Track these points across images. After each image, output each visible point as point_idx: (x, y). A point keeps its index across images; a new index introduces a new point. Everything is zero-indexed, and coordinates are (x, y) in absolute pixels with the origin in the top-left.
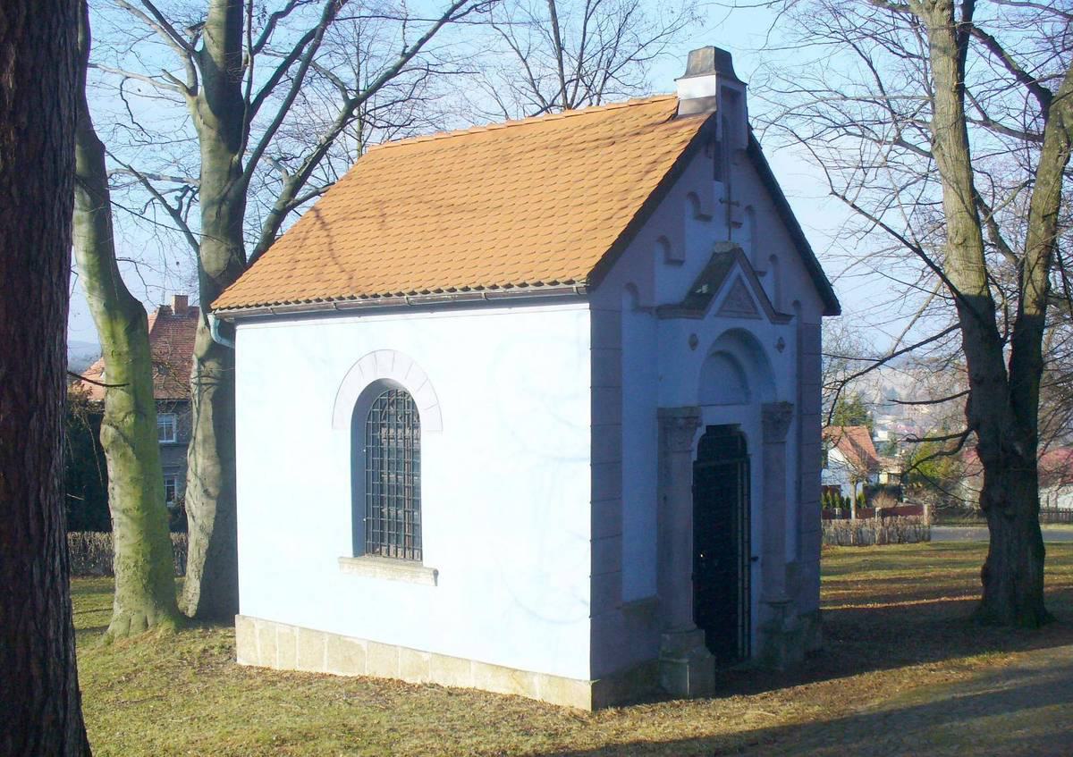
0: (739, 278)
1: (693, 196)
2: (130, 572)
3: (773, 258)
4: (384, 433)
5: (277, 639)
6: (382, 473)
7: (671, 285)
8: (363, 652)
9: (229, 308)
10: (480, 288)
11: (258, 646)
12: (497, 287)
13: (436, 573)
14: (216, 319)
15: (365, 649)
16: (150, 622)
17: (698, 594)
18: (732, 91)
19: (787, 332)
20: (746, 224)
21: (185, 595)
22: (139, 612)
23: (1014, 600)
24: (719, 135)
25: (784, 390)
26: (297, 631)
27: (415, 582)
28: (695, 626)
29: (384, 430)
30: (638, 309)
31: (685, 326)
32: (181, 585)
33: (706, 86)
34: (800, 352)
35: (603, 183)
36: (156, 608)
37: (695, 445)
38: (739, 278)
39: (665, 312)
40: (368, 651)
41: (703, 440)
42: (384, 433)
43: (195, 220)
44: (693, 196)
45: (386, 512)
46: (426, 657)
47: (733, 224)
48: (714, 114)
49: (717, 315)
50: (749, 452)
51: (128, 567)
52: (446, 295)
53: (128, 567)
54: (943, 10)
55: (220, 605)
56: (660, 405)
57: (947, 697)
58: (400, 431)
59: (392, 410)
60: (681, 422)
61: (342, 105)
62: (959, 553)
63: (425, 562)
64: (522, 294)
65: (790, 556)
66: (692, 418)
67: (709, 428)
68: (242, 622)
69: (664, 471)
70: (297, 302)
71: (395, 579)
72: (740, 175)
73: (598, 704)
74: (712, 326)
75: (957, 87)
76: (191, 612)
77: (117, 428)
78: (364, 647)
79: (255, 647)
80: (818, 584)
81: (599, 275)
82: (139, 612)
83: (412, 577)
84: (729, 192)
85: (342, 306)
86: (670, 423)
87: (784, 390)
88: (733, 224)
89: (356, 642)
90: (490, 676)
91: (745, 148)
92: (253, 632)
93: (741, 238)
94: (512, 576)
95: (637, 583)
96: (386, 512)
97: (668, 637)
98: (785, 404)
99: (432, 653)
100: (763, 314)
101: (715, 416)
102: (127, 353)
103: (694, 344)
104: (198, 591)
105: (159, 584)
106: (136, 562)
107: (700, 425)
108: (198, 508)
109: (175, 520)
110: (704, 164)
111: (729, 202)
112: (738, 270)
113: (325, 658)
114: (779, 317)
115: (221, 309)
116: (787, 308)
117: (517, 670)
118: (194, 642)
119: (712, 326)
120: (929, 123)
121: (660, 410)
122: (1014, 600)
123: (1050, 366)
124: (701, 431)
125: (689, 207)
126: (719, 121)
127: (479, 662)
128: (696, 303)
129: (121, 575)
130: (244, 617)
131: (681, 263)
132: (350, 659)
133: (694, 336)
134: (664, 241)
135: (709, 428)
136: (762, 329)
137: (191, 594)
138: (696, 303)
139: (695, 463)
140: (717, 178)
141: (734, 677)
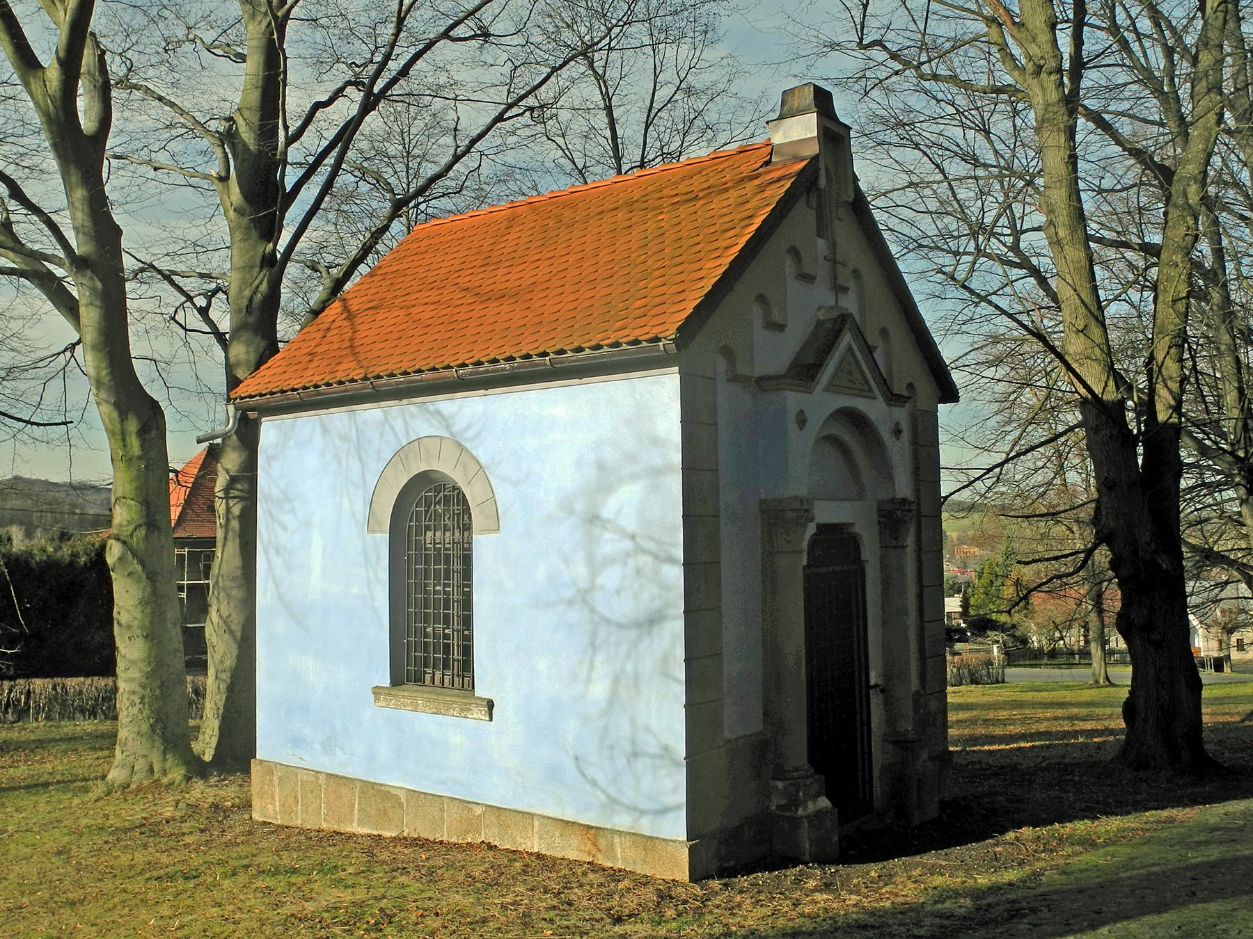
0: (850, 349)
1: (794, 252)
2: (135, 710)
3: (884, 333)
4: (430, 534)
6: (426, 585)
8: (401, 804)
9: (251, 397)
10: (545, 354)
11: (277, 798)
12: (565, 352)
13: (490, 705)
14: (236, 409)
16: (156, 768)
17: (811, 731)
18: (834, 136)
19: (901, 415)
20: (852, 284)
21: (201, 737)
22: (145, 756)
23: (1168, 745)
24: (823, 182)
25: (903, 487)
26: (322, 778)
28: (812, 770)
29: (429, 534)
30: (734, 378)
31: (793, 399)
32: (197, 729)
33: (803, 129)
34: (915, 442)
35: (651, 323)
36: (164, 753)
37: (805, 545)
38: (850, 349)
39: (763, 384)
41: (814, 543)
42: (430, 534)
43: (224, 320)
44: (794, 252)
45: (431, 645)
46: (478, 811)
47: (840, 289)
48: (815, 159)
49: (826, 390)
51: (133, 704)
52: (504, 365)
53: (133, 704)
54: (1050, 73)
55: (237, 750)
56: (763, 496)
57: (1214, 853)
58: (448, 534)
59: (440, 509)
60: (790, 515)
61: (388, 205)
62: (1092, 691)
63: (480, 691)
64: (595, 358)
65: (915, 684)
66: (803, 511)
67: (819, 526)
68: (258, 767)
69: (770, 578)
70: (328, 384)
72: (845, 229)
74: (821, 402)
75: (1070, 156)
76: (208, 757)
77: (124, 543)
78: (402, 795)
80: (945, 725)
81: (687, 332)
82: (145, 756)
83: (462, 710)
84: (834, 248)
85: (380, 386)
87: (903, 487)
88: (840, 289)
89: (393, 791)
90: (557, 834)
91: (851, 200)
93: (849, 303)
94: (580, 707)
95: (740, 720)
96: (431, 645)
97: (780, 784)
98: (904, 501)
99: (486, 806)
100: (877, 392)
101: (826, 513)
102: (140, 458)
103: (802, 421)
104: (216, 732)
105: (171, 733)
106: (142, 698)
107: (812, 520)
108: (220, 649)
109: (140, 577)
110: (804, 215)
111: (833, 261)
112: (847, 339)
113: (356, 812)
114: (894, 399)
115: (242, 398)
116: (899, 388)
117: (592, 827)
118: (202, 792)
119: (821, 402)
121: (763, 502)
122: (1168, 745)
124: (811, 529)
125: (789, 265)
126: (822, 165)
127: (543, 817)
128: (805, 371)
129: (125, 713)
130: (261, 761)
131: (781, 327)
133: (802, 412)
134: (762, 299)
135: (819, 526)
136: (876, 409)
137: (206, 746)
138: (805, 371)
139: (804, 568)
140: (820, 233)
141: (871, 834)
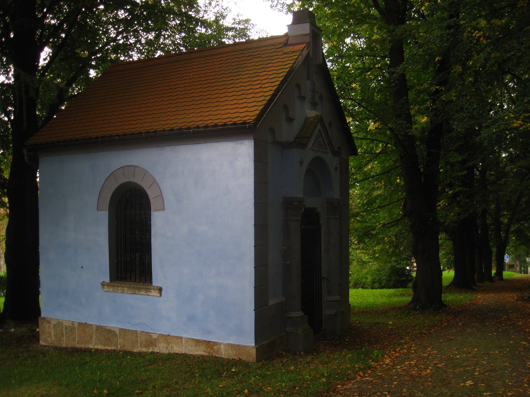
5: (64, 330)
7: (288, 132)
8: (116, 335)
11: (53, 334)
13: (160, 290)
15: (118, 333)
27: (148, 295)
40: (120, 334)
46: (155, 336)
50: (321, 223)
63: (155, 283)
71: (136, 294)
73: (258, 360)
79: (51, 334)
86: (288, 204)
92: (49, 326)
120: (522, 80)
123: (401, 207)
128: (300, 142)
130: (44, 318)
132: (109, 339)
